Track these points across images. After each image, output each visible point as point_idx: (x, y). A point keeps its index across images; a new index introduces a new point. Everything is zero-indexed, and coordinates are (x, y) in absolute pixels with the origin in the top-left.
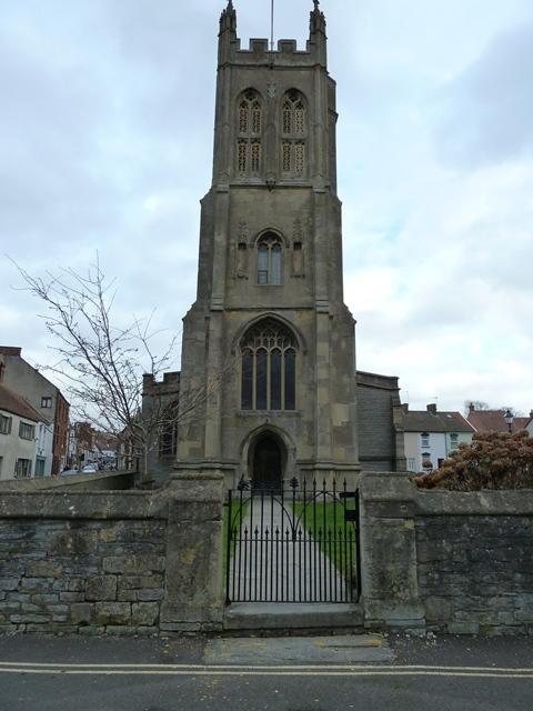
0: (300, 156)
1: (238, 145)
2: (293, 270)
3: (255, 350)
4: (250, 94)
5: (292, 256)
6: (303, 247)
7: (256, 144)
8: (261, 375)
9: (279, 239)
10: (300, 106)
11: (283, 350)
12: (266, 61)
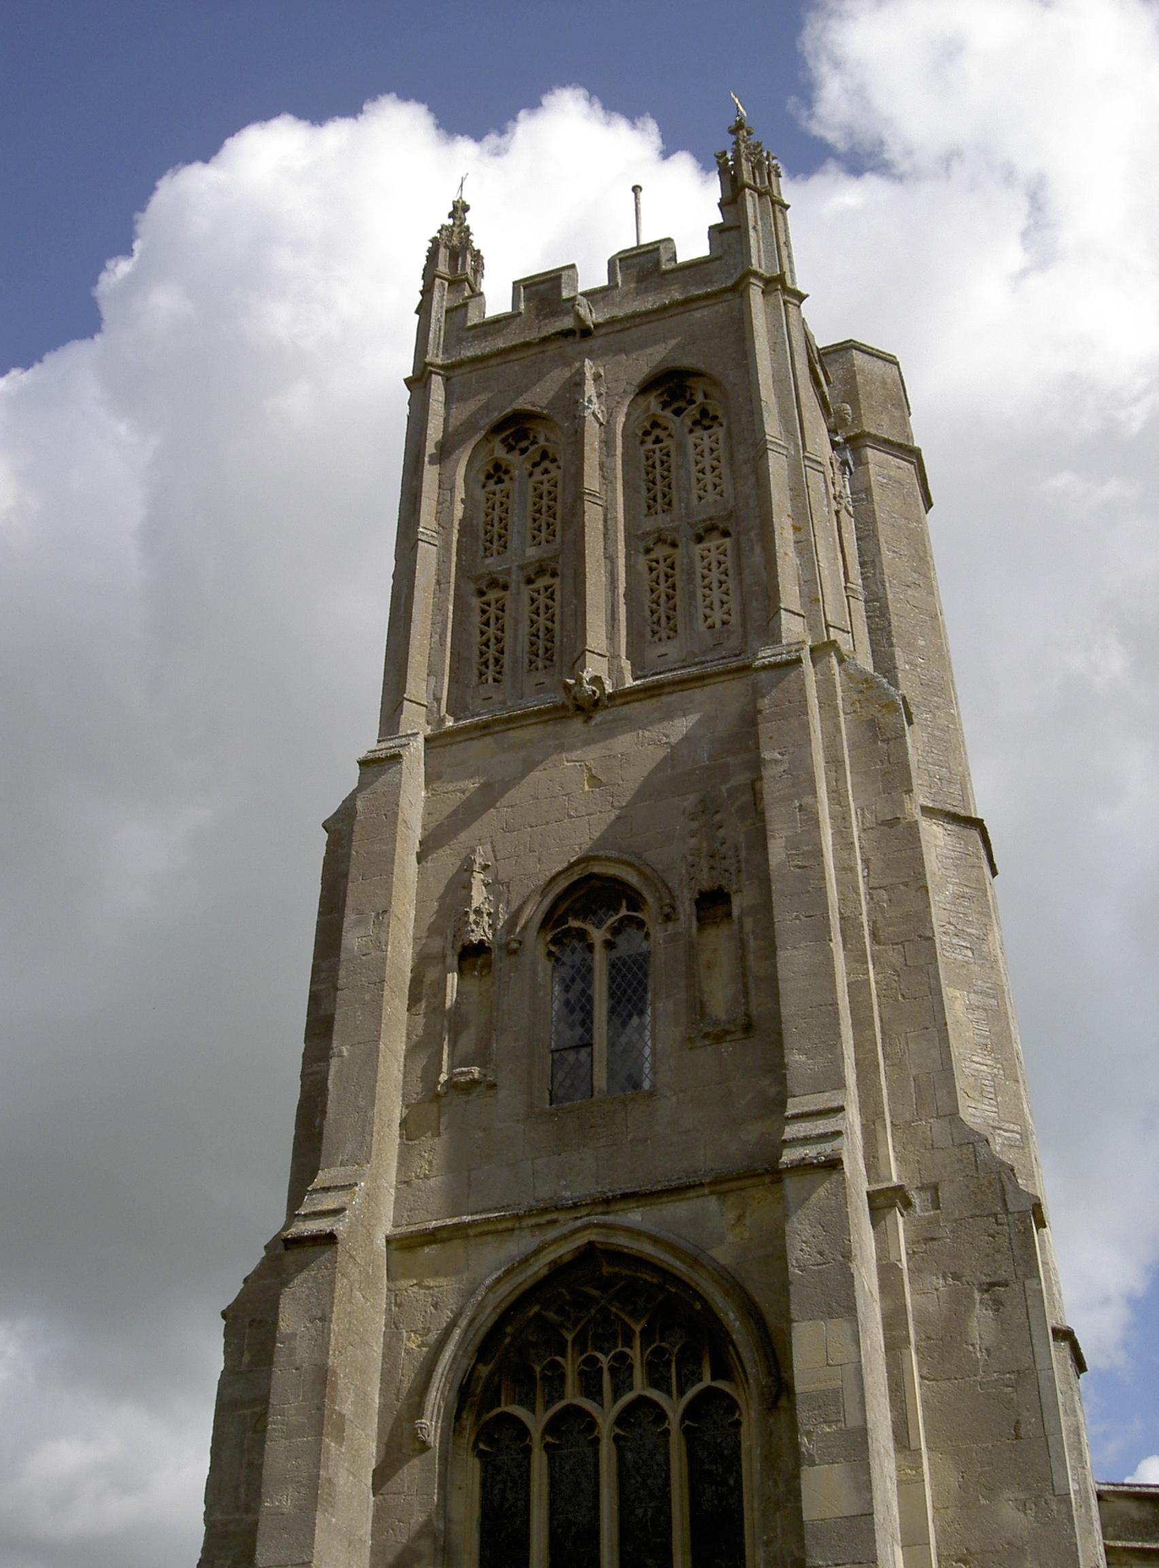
0: (715, 575)
1: (476, 602)
2: (698, 1008)
3: (535, 1421)
4: (522, 435)
5: (692, 950)
6: (738, 904)
7: (541, 583)
8: (574, 1491)
9: (635, 902)
10: (705, 419)
11: (674, 1408)
12: (567, 322)
